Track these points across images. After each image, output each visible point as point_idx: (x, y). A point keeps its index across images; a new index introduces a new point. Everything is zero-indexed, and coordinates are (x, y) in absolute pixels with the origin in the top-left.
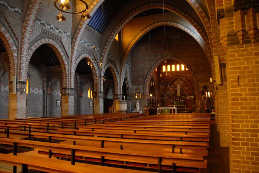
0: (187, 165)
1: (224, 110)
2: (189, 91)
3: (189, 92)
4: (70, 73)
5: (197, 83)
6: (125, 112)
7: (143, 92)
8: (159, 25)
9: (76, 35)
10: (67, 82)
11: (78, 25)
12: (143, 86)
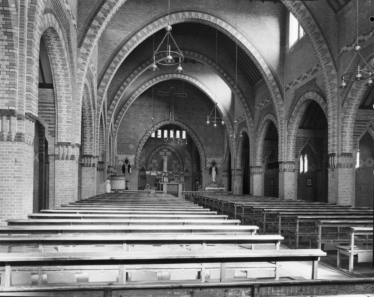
0: (164, 256)
2: (177, 165)
5: (205, 157)
7: (134, 164)
8: (174, 78)
12: (134, 156)
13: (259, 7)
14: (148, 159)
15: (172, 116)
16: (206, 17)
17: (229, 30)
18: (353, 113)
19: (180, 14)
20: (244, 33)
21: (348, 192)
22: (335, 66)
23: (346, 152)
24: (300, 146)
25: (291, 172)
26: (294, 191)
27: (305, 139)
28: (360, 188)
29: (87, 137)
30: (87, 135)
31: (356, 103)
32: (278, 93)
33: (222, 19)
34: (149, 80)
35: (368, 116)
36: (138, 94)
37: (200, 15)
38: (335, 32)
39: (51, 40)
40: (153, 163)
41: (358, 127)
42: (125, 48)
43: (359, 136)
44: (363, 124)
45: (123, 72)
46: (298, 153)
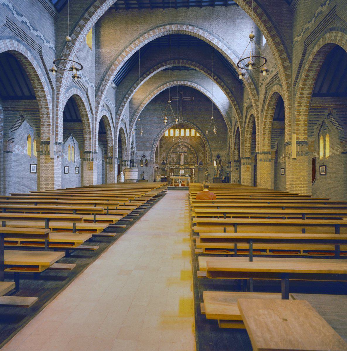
1: (295, 180)
3: (193, 160)
4: (94, 134)
5: (211, 151)
6: (136, 181)
7: (150, 159)
9: (101, 88)
10: (92, 145)
11: (105, 75)
12: (150, 152)
13: (234, 12)
14: (168, 154)
15: (181, 117)
16: (184, 28)
17: (206, 36)
18: (306, 101)
19: (162, 28)
20: (220, 38)
21: (303, 179)
22: (288, 58)
23: (300, 140)
24: (277, 137)
25: (267, 161)
26: (270, 180)
27: (281, 130)
28: (330, 176)
29: (87, 137)
30: (86, 135)
31: (308, 92)
32: (254, 89)
33: (199, 28)
34: (157, 88)
35: (325, 104)
36: (148, 100)
37: (179, 27)
38: (288, 24)
39: (22, 60)
40: (172, 158)
41: (315, 115)
42: (116, 62)
43: (316, 124)
44: (320, 112)
45: (128, 83)
46: (275, 143)
